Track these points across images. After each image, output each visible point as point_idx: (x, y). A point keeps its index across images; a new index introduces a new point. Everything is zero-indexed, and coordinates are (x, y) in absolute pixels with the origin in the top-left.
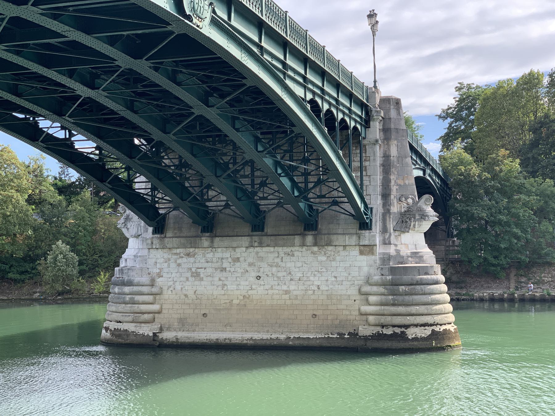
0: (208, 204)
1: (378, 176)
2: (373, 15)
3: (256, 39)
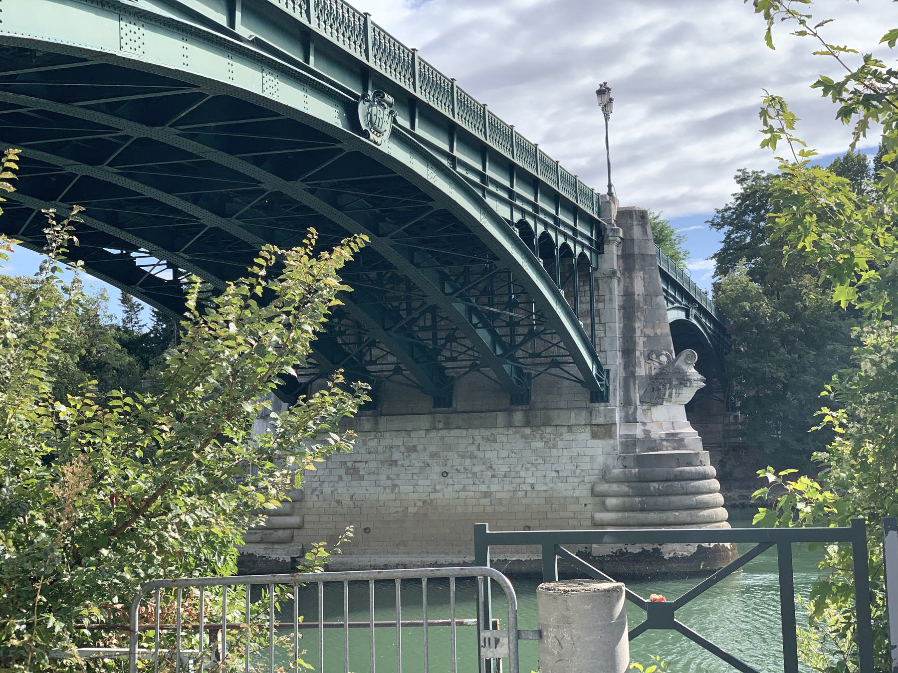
0: (369, 368)
1: (617, 324)
2: (604, 91)
3: (446, 148)
